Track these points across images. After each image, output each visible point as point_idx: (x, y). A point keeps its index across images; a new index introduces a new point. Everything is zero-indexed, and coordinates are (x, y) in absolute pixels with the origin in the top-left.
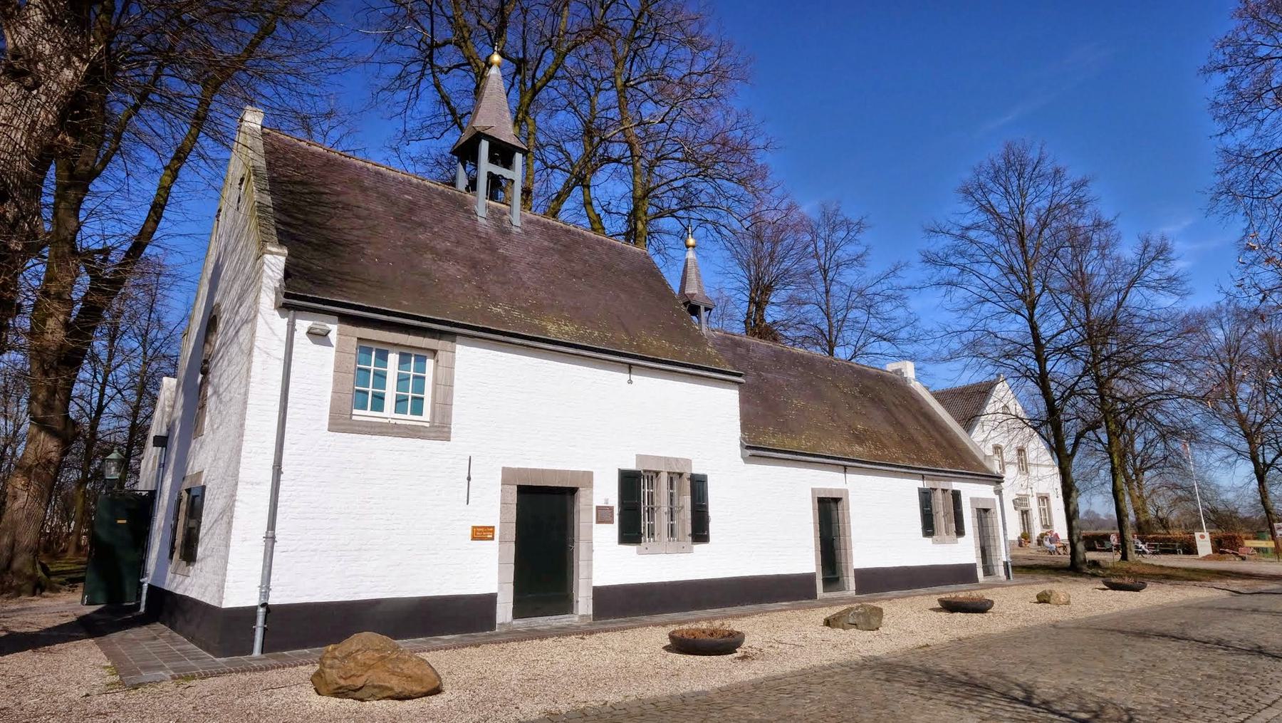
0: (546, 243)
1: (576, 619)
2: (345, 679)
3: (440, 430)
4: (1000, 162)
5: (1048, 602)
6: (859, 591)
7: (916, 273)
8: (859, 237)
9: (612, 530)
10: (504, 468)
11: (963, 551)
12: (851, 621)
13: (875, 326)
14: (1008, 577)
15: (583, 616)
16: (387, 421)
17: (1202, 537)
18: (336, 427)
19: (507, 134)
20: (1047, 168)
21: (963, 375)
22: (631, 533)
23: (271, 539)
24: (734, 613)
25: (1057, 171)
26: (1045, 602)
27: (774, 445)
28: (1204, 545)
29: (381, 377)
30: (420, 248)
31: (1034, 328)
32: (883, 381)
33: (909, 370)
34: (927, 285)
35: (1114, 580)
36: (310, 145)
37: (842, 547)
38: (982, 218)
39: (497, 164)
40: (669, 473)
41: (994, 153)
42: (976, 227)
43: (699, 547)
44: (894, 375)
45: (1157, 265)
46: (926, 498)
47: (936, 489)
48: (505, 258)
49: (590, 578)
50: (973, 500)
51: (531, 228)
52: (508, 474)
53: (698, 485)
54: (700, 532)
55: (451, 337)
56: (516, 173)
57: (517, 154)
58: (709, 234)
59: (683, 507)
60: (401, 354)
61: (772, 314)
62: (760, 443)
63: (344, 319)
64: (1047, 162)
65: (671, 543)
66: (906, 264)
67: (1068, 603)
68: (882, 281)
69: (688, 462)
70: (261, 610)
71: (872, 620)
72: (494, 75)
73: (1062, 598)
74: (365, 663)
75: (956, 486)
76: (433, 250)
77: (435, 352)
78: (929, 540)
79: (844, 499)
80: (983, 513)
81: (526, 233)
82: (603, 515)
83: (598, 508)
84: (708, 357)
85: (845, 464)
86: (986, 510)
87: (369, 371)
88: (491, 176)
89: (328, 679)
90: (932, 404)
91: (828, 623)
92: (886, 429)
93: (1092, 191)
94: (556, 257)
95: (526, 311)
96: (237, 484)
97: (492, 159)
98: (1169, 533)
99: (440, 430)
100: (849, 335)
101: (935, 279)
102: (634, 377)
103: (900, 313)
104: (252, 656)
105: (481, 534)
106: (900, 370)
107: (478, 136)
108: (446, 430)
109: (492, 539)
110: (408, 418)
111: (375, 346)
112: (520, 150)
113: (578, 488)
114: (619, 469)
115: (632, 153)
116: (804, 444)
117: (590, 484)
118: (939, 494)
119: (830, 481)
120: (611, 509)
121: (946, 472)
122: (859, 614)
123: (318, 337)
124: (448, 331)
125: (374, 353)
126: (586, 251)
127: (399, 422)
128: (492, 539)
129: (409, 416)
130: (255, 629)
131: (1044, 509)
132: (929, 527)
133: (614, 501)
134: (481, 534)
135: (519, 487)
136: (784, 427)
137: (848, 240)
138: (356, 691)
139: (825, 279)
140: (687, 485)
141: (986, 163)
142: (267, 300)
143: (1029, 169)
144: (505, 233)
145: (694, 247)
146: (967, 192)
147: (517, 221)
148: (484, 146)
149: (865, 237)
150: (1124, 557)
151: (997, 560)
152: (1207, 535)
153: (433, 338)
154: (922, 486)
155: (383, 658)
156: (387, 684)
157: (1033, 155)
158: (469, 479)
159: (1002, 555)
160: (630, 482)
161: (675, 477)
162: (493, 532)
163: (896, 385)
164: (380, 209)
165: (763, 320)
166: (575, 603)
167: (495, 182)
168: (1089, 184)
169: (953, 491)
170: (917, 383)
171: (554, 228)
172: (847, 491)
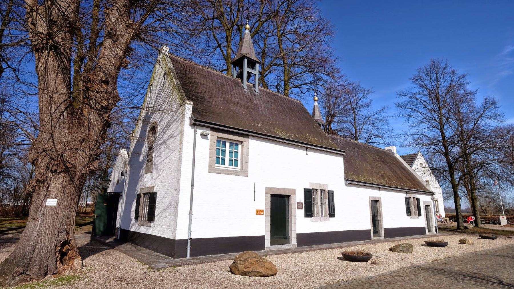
0: (268, 99)
1: (291, 246)
2: (245, 269)
3: (244, 172)
4: (428, 68)
5: (465, 243)
6: (385, 237)
7: (393, 111)
8: (368, 96)
9: (302, 212)
10: (266, 188)
11: (420, 222)
12: (401, 250)
13: (375, 132)
14: (437, 233)
15: (293, 245)
16: (227, 169)
17: (503, 218)
18: (212, 171)
19: (254, 57)
20: (449, 70)
21: (409, 151)
22: (309, 213)
23: (191, 213)
24: (347, 245)
25: (453, 72)
26: (463, 243)
27: (355, 179)
28: (504, 221)
29: (224, 151)
30: (229, 101)
31: (442, 133)
32: (385, 154)
33: (394, 150)
34: (398, 116)
35: (483, 235)
36: (184, 60)
37: (379, 219)
38: (421, 90)
39: (250, 68)
40: (320, 190)
41: (426, 63)
42: (419, 93)
44: (388, 151)
45: (491, 109)
46: (407, 200)
47: (411, 197)
48: (256, 105)
50: (424, 202)
51: (262, 93)
52: (268, 189)
53: (331, 194)
54: (332, 214)
55: (247, 136)
56: (256, 72)
57: (257, 64)
58: (310, 94)
59: (325, 203)
60: (230, 143)
61: (334, 126)
62: (350, 179)
63: (213, 129)
64: (448, 68)
65: (322, 217)
66: (387, 107)
67: (473, 244)
68: (378, 114)
69: (327, 185)
70: (189, 241)
71: (409, 249)
72: (247, 33)
73: (471, 242)
74: (251, 263)
75: (418, 196)
76: (232, 102)
77: (242, 142)
78: (409, 217)
79: (380, 201)
81: (261, 95)
82: (299, 207)
83: (297, 203)
84: (331, 144)
85: (380, 187)
86: (376, 201)
87: (220, 149)
88: (248, 72)
89: (240, 268)
90: (240, 153)
91: (391, 250)
92: (390, 173)
93: (467, 79)
94: (273, 104)
95: (268, 126)
96: (179, 192)
97: (248, 67)
98: (486, 216)
99: (244, 172)
100: (364, 135)
101: (401, 114)
102: (308, 152)
103: (385, 127)
104: (187, 258)
105: (259, 213)
106: (391, 150)
107: (243, 57)
108: (247, 172)
109: (263, 215)
110: (233, 168)
111: (221, 140)
112: (259, 63)
113: (290, 195)
114: (305, 189)
115: (284, 63)
116: (365, 180)
117: (294, 194)
118: (412, 199)
119: (375, 193)
120: (302, 203)
121: (415, 191)
122: (404, 247)
123: (204, 136)
125: (221, 142)
126: (281, 102)
127: (231, 169)
129: (233, 167)
130: (187, 248)
131: (436, 205)
132: (409, 212)
133: (303, 201)
134: (259, 213)
135: (271, 195)
136: (357, 172)
137: (363, 97)
138: (248, 273)
139: (354, 112)
141: (423, 68)
143: (441, 70)
144: (254, 95)
145: (317, 100)
146: (415, 80)
147: (257, 91)
148: (246, 61)
149: (370, 96)
150: (476, 225)
151: (432, 225)
152: (505, 217)
153: (242, 137)
154: (406, 196)
155: (257, 261)
156: (260, 271)
157: (443, 65)
158: (255, 191)
159: (434, 224)
160: (309, 193)
161: (323, 191)
162: (263, 212)
163: (389, 155)
164: (212, 86)
165: (331, 128)
166: (290, 240)
167: (249, 74)
168: (466, 77)
169: (329, 191)
170: (398, 155)
171: (269, 93)
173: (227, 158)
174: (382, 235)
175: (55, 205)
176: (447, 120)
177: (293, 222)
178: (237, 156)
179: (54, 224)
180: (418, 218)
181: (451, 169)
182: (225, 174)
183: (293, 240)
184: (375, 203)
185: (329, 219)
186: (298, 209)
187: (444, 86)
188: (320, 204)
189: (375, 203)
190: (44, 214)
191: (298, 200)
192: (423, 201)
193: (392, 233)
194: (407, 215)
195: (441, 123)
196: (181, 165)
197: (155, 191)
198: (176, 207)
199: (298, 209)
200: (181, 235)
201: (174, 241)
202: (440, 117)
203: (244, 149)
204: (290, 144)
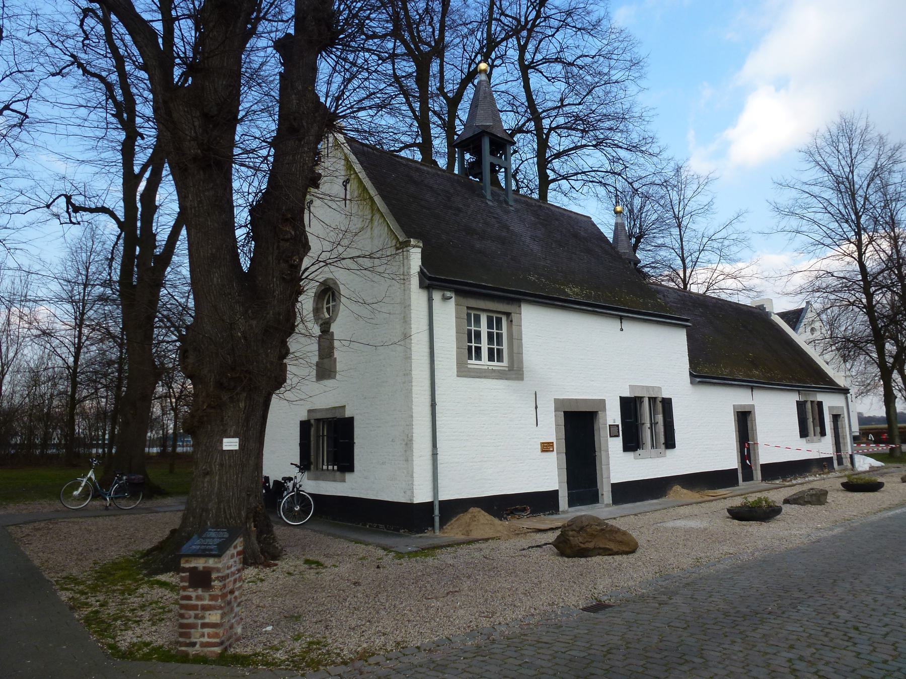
2: (584, 543)
11: (823, 448)
16: (486, 367)
22: (632, 443)
29: (478, 335)
43: (669, 452)
46: (801, 406)
49: (609, 477)
50: (830, 408)
52: (559, 403)
53: (667, 404)
54: (670, 443)
66: (746, 212)
75: (820, 397)
80: (836, 418)
85: (752, 384)
113: (596, 412)
117: (604, 409)
118: (809, 405)
119: (741, 397)
120: (618, 426)
124: (518, 297)
127: (494, 368)
128: (553, 451)
132: (804, 433)
133: (618, 422)
134: (546, 447)
140: (659, 406)
142: (415, 281)
158: (536, 408)
160: (629, 406)
161: (652, 400)
166: (600, 495)
169: (663, 399)
172: (753, 406)
173: (484, 346)
174: (757, 478)
175: (237, 448)
176: (871, 240)
177: (603, 463)
178: (499, 343)
179: (239, 480)
180: (820, 441)
181: (878, 339)
182: (485, 377)
183: (605, 496)
184: (744, 419)
185: (665, 454)
186: (611, 436)
187: (864, 168)
188: (649, 425)
189: (744, 419)
190: (221, 465)
191: (610, 422)
192: (829, 407)
193: (774, 471)
194: (801, 437)
195: (859, 245)
196: (411, 366)
197: (348, 414)
198: (406, 444)
199: (611, 436)
200: (422, 495)
201: (412, 504)
202: (858, 234)
203: (514, 327)
204: (593, 311)
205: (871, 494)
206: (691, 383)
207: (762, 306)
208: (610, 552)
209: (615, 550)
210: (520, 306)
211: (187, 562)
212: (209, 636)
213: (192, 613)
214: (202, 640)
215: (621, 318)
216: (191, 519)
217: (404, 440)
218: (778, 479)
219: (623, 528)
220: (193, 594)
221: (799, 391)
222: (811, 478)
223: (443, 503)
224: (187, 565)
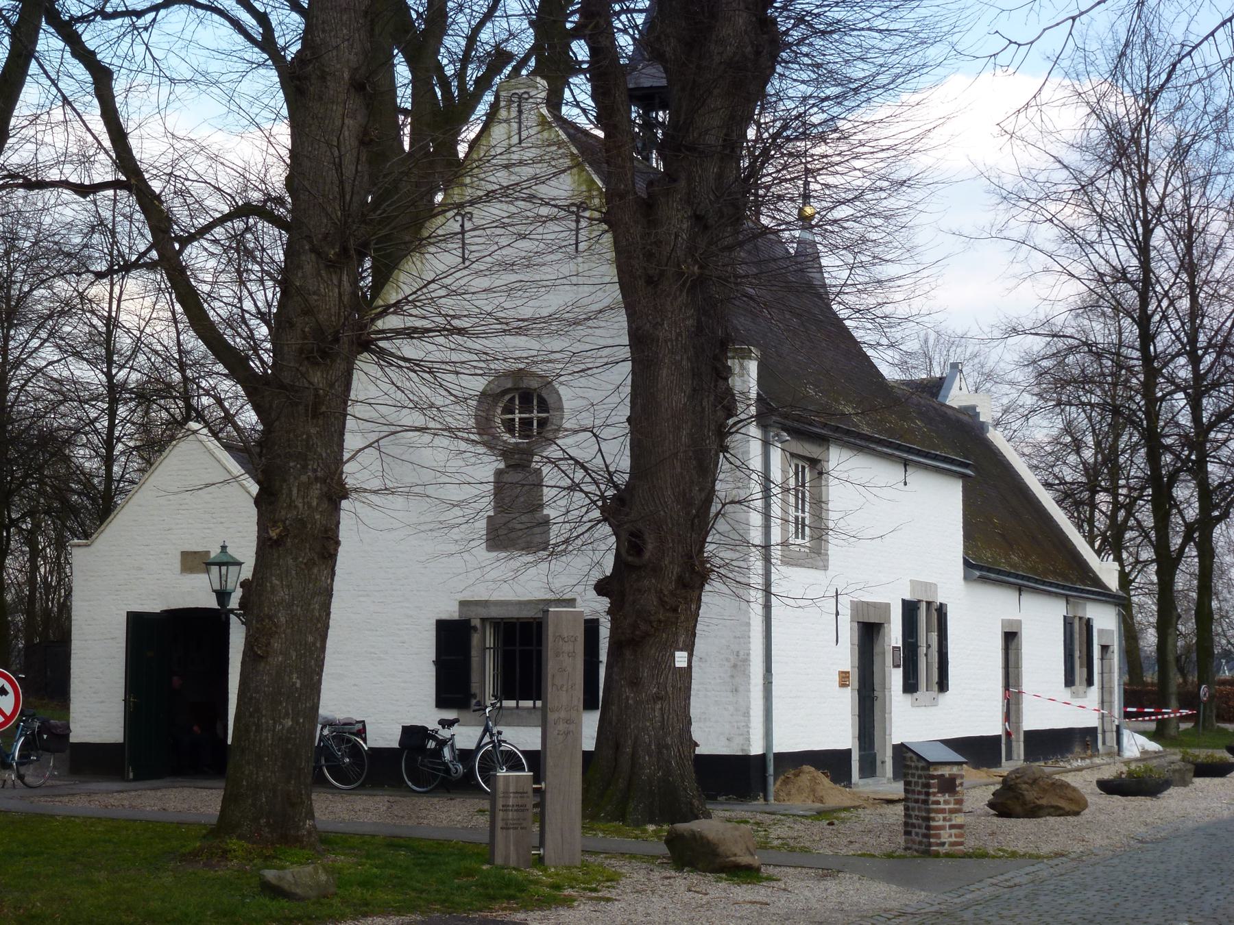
132: (1069, 681)
133: (900, 644)
161: (929, 604)
166: (878, 763)
172: (1020, 622)
205: (1217, 780)
206: (966, 578)
207: (973, 408)
208: (1061, 812)
209: (1067, 809)
210: (828, 449)
211: (935, 770)
212: (956, 836)
213: (941, 816)
214: (950, 840)
215: (906, 464)
216: (647, 758)
217: (728, 660)
218: (1038, 760)
219: (1073, 784)
220: (942, 800)
221: (1067, 597)
222: (1079, 763)
223: (780, 757)
224: (936, 773)
